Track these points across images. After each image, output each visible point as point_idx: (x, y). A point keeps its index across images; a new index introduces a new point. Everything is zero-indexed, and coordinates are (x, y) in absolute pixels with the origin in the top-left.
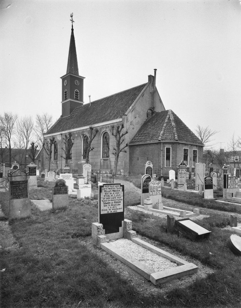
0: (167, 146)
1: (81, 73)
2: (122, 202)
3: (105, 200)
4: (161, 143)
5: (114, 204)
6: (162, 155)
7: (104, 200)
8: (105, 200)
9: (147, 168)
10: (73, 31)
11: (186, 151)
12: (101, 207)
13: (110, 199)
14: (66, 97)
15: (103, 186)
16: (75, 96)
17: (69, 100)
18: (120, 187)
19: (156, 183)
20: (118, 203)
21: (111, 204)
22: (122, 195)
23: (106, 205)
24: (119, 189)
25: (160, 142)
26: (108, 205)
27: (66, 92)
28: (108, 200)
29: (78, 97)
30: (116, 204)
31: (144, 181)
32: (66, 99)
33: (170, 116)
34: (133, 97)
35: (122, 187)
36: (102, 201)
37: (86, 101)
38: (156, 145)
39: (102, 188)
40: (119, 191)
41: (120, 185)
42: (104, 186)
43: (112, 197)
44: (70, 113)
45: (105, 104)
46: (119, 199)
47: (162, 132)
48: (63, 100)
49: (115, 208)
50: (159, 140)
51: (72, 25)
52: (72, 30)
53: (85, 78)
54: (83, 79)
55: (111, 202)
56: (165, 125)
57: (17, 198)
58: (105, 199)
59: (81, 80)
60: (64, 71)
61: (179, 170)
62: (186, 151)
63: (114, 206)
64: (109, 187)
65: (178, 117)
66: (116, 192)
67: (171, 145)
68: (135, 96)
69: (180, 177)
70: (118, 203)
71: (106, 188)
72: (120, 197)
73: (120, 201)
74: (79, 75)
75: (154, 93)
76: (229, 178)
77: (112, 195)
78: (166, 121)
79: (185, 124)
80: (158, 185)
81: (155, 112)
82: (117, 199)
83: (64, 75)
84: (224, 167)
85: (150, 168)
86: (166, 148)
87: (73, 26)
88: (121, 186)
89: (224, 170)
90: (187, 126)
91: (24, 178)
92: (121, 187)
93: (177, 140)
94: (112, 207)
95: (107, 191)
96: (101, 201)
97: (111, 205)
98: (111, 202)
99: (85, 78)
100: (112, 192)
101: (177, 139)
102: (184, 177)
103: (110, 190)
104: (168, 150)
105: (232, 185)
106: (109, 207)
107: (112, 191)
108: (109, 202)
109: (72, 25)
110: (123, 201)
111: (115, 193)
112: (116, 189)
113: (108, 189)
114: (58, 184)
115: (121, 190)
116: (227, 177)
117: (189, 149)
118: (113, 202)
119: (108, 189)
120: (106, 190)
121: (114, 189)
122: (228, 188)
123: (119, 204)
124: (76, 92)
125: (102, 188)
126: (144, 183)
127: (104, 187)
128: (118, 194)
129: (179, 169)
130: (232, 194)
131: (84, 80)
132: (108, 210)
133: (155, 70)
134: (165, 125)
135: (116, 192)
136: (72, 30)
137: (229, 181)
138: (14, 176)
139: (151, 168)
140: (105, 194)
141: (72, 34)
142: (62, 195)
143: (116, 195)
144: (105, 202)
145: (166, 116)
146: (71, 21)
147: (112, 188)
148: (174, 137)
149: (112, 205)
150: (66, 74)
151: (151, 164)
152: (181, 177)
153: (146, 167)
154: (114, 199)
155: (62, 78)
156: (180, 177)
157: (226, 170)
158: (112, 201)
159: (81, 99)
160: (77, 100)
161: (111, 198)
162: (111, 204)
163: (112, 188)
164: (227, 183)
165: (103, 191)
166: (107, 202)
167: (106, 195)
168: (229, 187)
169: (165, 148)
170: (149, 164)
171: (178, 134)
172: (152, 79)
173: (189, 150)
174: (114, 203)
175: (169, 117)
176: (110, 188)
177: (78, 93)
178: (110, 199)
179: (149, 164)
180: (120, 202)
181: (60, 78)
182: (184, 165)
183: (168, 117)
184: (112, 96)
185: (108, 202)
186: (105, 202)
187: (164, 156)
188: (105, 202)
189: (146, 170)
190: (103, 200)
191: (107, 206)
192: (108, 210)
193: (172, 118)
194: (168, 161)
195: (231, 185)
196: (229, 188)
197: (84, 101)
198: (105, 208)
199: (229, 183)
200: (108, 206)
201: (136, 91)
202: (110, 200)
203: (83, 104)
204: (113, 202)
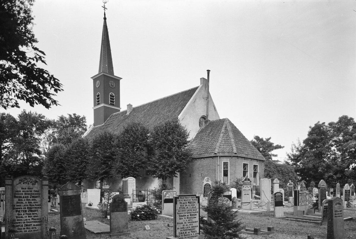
0: (226, 160)
1: (116, 73)
2: (198, 214)
3: (180, 212)
4: (218, 156)
5: (190, 217)
6: (219, 171)
7: (179, 213)
8: (180, 212)
9: (205, 185)
10: (106, 21)
11: (245, 165)
12: (177, 220)
13: (185, 212)
14: (98, 101)
15: (178, 198)
16: (111, 101)
17: (102, 105)
18: (195, 198)
19: (225, 200)
20: (194, 216)
21: (186, 217)
22: (198, 207)
23: (182, 217)
24: (194, 201)
25: (216, 155)
26: (183, 217)
27: (98, 96)
28: (183, 212)
29: (113, 102)
30: (192, 217)
31: (210, 197)
32: (98, 104)
33: (227, 125)
34: (182, 102)
35: (197, 199)
36: (178, 213)
37: (123, 107)
38: (211, 159)
39: (177, 199)
40: (195, 202)
41: (195, 197)
42: (180, 197)
43: (188, 210)
44: (105, 120)
45: (149, 110)
46: (194, 211)
47: (218, 144)
48: (95, 105)
49: (191, 221)
50: (215, 154)
51: (105, 13)
52: (105, 19)
53: (122, 78)
54: (119, 81)
55: (186, 214)
56: (222, 135)
57: (69, 215)
58: (180, 211)
59: (117, 81)
60: (95, 71)
61: (243, 187)
62: (245, 165)
63: (190, 219)
64: (185, 198)
65: (236, 127)
66: (191, 204)
67: (228, 159)
68: (186, 101)
69: (244, 195)
70: (194, 216)
71: (182, 199)
72: (195, 209)
73: (196, 214)
74: (115, 75)
75: (208, 98)
76: (300, 195)
77: (188, 207)
78: (223, 130)
79: (244, 135)
80: (227, 202)
81: (208, 120)
82: (193, 211)
83: (95, 75)
84: (289, 183)
85: (208, 186)
86: (223, 162)
87: (106, 14)
88: (197, 197)
89: (289, 187)
90: (246, 137)
91: (75, 192)
92: (196, 199)
93: (236, 154)
94: (187, 220)
95: (182, 203)
96: (177, 213)
97: (186, 218)
98: (186, 214)
99: (122, 78)
100: (188, 204)
101: (236, 153)
102: (248, 194)
103: (185, 201)
104: (226, 164)
105: (302, 202)
106: (185, 220)
107: (187, 203)
108: (185, 214)
109: (105, 13)
110: (198, 214)
111: (190, 205)
112: (191, 201)
113: (183, 200)
114: (117, 200)
115: (197, 202)
116: (297, 193)
117: (249, 164)
118: (189, 214)
119: (183, 200)
120: (181, 201)
121: (190, 201)
122: (299, 205)
123: (195, 216)
124: (111, 96)
125: (177, 199)
126: (211, 199)
127: (180, 199)
128: (194, 206)
129: (244, 186)
130: (304, 211)
131: (121, 81)
132: (184, 223)
133: (208, 71)
134: (222, 135)
135: (191, 204)
136: (105, 19)
137: (300, 197)
138: (65, 190)
139: (210, 185)
140: (181, 206)
141: (105, 25)
142: (121, 212)
143: (191, 207)
144: (180, 215)
145: (222, 125)
146: (104, 8)
147: (187, 200)
148: (233, 150)
149: (187, 218)
150: (98, 73)
151: (210, 181)
152: (246, 194)
153: (204, 184)
154: (190, 211)
155: (94, 78)
156: (244, 195)
157: (291, 187)
158: (187, 213)
159: (118, 105)
160: (113, 105)
161: (186, 210)
162: (186, 217)
163: (187, 200)
164: (298, 200)
165: (178, 203)
166: (182, 215)
167: (182, 207)
168: (300, 204)
169: (223, 162)
170: (208, 181)
171: (236, 146)
172: (206, 82)
173: (249, 165)
174: (189, 215)
175: (226, 127)
176: (186, 199)
177: (113, 96)
178: (185, 212)
179: (207, 180)
180: (196, 215)
181: (91, 78)
182: (248, 180)
183: (224, 126)
184: (157, 102)
185: (183, 214)
186: (181, 215)
187: (221, 172)
188: (181, 215)
189: (204, 187)
190: (178, 212)
191: (182, 218)
192: (184, 223)
193: (229, 128)
194: (225, 178)
195: (302, 202)
196: (300, 205)
197: (121, 106)
198: (181, 221)
199: (300, 200)
200: (183, 218)
201: (186, 96)
202: (185, 213)
203: (119, 111)
204: (189, 214)
